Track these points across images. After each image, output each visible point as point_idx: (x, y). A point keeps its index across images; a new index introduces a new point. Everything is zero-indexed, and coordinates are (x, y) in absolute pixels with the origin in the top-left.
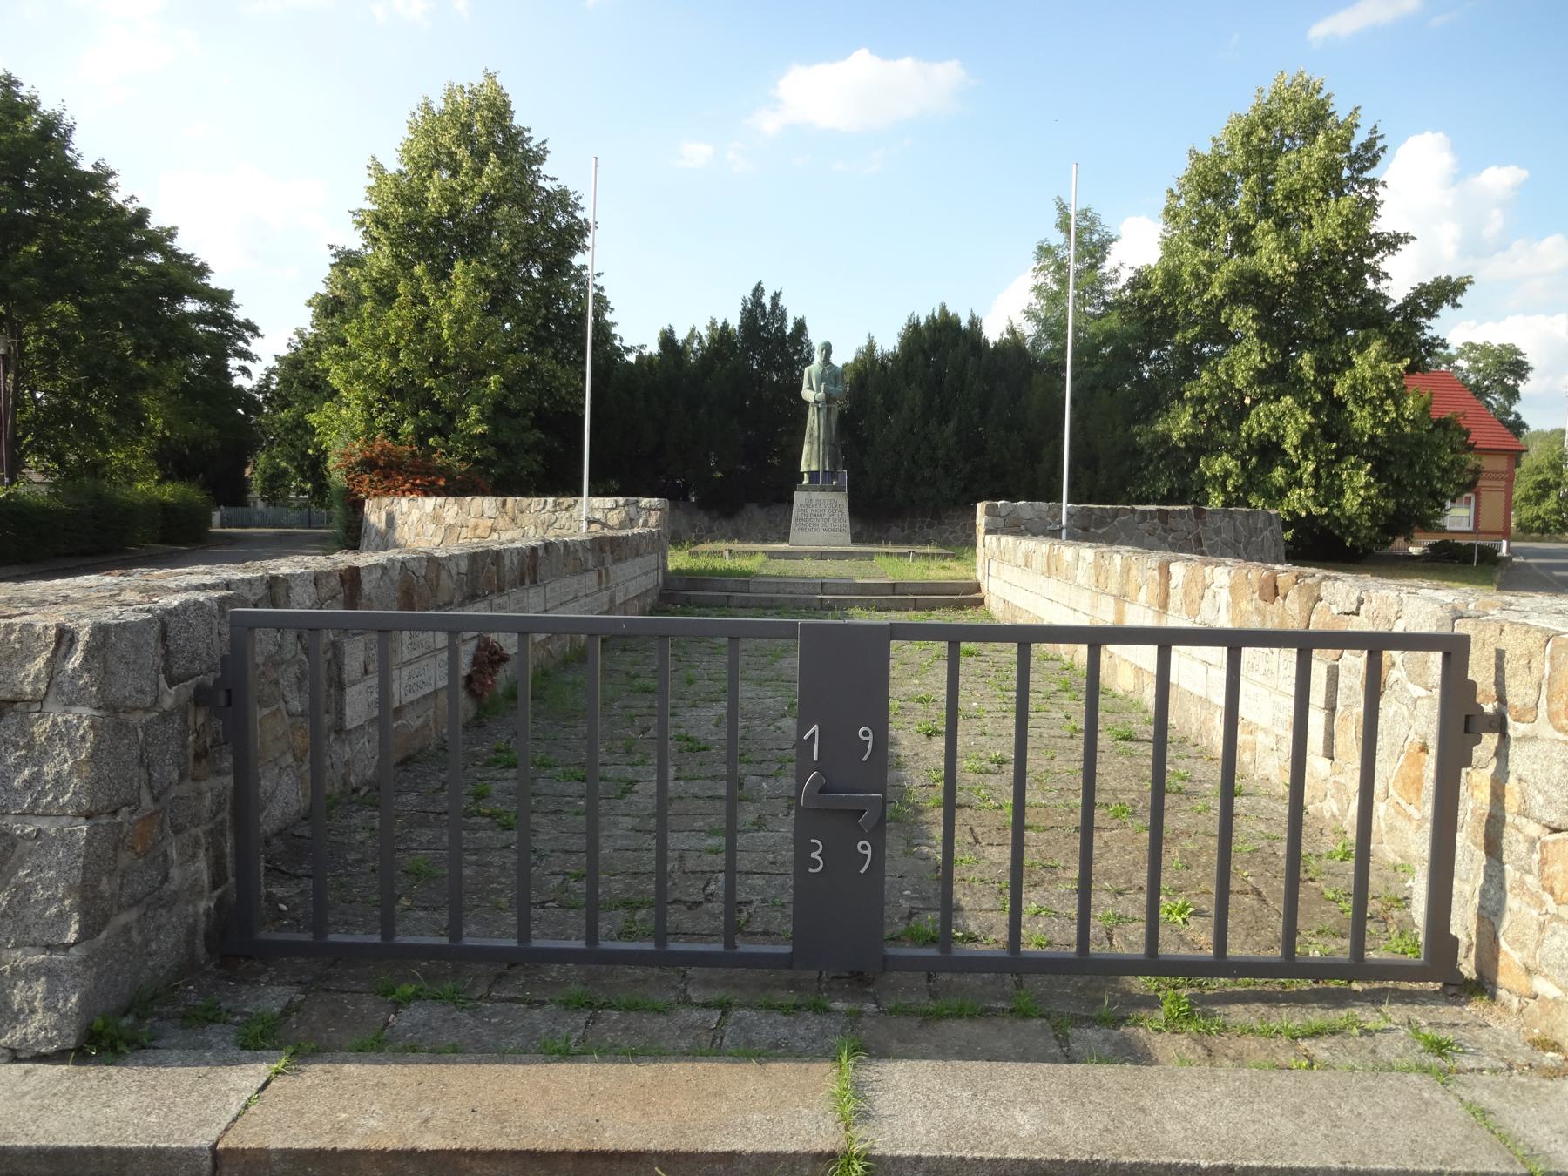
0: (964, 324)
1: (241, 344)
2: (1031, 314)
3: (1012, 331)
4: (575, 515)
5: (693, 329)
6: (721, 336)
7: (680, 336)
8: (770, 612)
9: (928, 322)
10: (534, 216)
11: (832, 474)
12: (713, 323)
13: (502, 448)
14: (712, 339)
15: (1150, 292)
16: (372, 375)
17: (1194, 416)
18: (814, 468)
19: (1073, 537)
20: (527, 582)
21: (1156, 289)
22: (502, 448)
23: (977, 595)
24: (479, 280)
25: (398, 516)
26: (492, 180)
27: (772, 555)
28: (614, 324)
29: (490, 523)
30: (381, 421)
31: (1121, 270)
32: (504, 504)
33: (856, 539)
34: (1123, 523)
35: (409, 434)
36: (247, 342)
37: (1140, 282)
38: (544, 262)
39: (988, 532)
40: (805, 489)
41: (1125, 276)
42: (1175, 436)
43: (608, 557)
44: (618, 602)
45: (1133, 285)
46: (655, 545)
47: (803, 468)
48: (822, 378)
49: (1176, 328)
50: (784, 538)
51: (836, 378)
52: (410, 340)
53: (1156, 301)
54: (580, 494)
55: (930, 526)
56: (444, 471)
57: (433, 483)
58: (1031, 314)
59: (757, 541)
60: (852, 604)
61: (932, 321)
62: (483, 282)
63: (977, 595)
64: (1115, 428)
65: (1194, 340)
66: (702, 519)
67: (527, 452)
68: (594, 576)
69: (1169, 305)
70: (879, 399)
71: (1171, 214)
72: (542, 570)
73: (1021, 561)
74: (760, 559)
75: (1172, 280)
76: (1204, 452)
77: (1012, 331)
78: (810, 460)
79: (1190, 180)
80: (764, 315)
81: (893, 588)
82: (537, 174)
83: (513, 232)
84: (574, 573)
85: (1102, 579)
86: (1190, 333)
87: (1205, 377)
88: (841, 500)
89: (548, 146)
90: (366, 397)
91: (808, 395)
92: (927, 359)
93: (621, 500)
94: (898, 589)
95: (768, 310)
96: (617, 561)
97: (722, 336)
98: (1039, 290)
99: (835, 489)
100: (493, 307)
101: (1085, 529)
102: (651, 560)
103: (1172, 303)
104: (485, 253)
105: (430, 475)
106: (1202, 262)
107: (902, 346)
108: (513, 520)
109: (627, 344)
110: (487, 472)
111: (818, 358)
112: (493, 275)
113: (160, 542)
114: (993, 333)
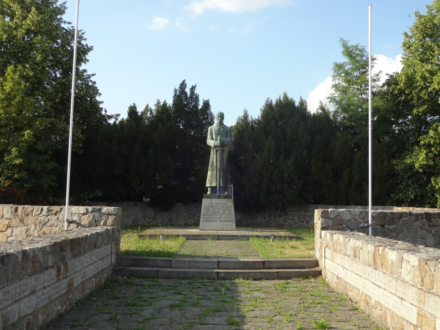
0: (297, 104)
2: (332, 99)
3: (322, 108)
4: (60, 218)
5: (147, 106)
6: (163, 110)
7: (140, 109)
8: (211, 178)
9: (277, 103)
10: (58, 43)
11: (225, 188)
12: (159, 103)
13: (32, 172)
14: (158, 111)
15: (398, 87)
17: (427, 154)
18: (214, 185)
19: (375, 234)
21: (402, 85)
22: (32, 172)
23: (316, 269)
24: (22, 77)
26: (33, 22)
27: (188, 237)
28: (102, 102)
29: (7, 222)
31: (380, 75)
32: (16, 210)
33: (239, 224)
34: (405, 222)
37: (392, 81)
38: (62, 68)
39: (323, 228)
40: (209, 197)
41: (384, 79)
42: (417, 165)
43: (68, 254)
44: (75, 284)
45: (388, 83)
46: (112, 237)
47: (208, 185)
48: (218, 133)
49: (413, 106)
50: (196, 225)
51: (226, 133)
53: (401, 92)
54: (65, 205)
55: (280, 216)
58: (332, 99)
59: (180, 226)
60: (237, 275)
61: (279, 102)
62: (26, 78)
63: (316, 269)
64: (383, 161)
65: (425, 113)
66: (151, 213)
67: (48, 174)
68: (54, 272)
69: (409, 94)
70: (251, 145)
71: (407, 46)
73: (351, 253)
74: (181, 240)
75: (410, 80)
76: (433, 174)
77: (322, 108)
78: (211, 180)
79: (417, 28)
80: (186, 98)
81: (263, 264)
82: (60, 20)
83: (43, 51)
84: (35, 272)
85: (427, 280)
86: (421, 109)
87: (431, 133)
88: (230, 204)
89: (66, 5)
91: (210, 142)
92: (277, 123)
93: (90, 208)
94: (267, 265)
95: (188, 96)
96: (75, 256)
97: (163, 109)
98: (336, 86)
99: (226, 197)
100: (30, 93)
101: (382, 226)
102: (106, 249)
103: (410, 93)
104: (27, 62)
106: (427, 70)
107: (263, 116)
108: (22, 220)
109: (109, 113)
111: (216, 121)
112: (31, 74)
114: (313, 108)
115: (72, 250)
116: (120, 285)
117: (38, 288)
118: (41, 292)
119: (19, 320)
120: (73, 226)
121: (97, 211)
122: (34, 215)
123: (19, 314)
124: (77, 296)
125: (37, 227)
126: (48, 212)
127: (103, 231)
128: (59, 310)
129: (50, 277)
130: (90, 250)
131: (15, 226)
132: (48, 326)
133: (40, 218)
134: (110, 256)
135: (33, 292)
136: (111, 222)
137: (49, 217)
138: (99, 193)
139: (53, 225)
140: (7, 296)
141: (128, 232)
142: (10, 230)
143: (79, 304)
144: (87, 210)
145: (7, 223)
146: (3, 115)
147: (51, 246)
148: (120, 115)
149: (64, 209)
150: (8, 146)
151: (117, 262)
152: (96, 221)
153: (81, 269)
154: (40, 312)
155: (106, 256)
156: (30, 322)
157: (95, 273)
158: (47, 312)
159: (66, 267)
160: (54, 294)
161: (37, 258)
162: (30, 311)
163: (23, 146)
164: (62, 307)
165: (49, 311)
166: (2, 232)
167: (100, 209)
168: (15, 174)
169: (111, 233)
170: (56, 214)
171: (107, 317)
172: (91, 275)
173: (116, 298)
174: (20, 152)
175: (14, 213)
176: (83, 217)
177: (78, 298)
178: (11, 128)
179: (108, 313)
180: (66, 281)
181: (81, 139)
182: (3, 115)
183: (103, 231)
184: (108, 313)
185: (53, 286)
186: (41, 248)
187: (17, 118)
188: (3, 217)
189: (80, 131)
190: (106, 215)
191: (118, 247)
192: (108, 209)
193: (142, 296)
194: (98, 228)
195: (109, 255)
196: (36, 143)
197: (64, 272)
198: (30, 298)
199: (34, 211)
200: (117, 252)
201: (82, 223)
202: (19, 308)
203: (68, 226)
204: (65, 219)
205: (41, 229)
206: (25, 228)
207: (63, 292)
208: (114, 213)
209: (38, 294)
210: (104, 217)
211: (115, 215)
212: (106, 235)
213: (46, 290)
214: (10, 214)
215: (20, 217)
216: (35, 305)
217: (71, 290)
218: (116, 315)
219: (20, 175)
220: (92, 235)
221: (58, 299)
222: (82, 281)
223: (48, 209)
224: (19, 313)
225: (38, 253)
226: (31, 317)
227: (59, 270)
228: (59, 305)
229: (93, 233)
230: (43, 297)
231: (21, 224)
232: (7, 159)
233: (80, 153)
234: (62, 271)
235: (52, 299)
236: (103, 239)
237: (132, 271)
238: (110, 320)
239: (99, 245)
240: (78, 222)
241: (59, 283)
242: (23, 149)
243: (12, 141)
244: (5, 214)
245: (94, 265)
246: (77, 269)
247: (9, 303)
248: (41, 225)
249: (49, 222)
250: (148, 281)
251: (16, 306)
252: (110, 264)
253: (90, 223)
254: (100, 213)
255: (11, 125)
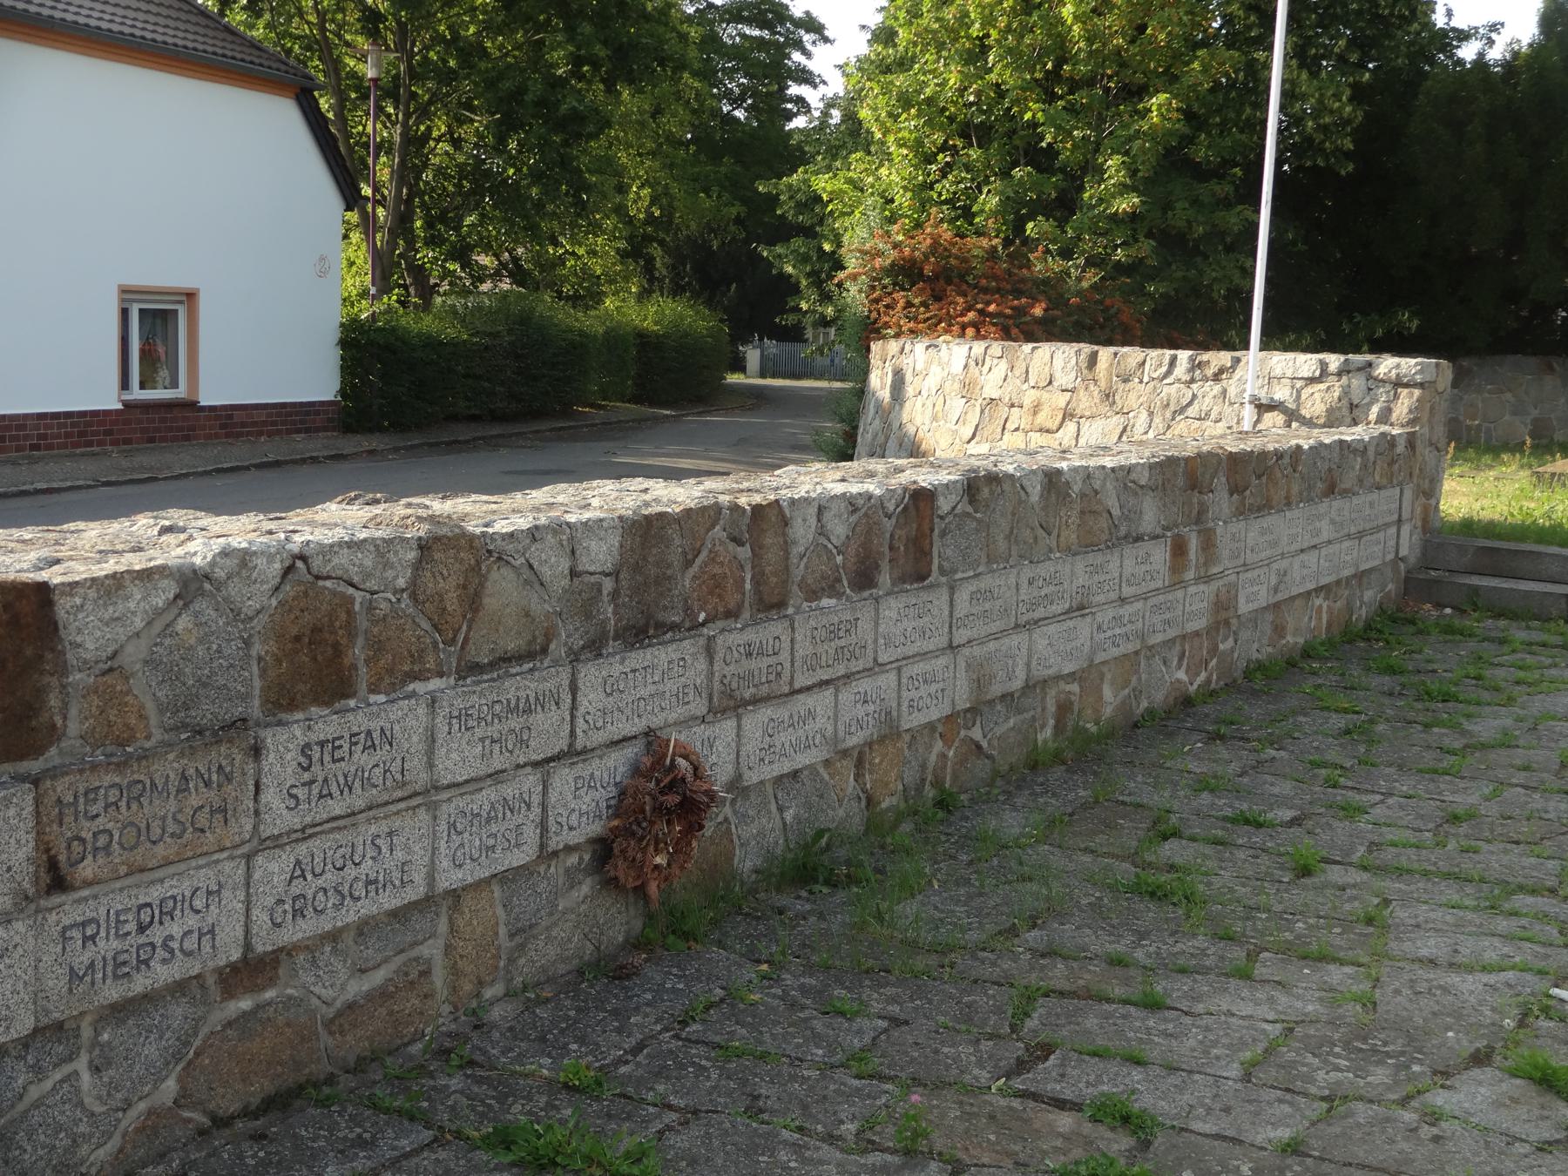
1: (797, 56)
4: (1232, 392)
16: (930, 101)
20: (885, 578)
25: (909, 377)
29: (1062, 400)
30: (946, 187)
32: (1093, 360)
35: (994, 214)
36: (808, 54)
46: (1404, 465)
52: (1008, 29)
54: (1247, 347)
56: (1050, 288)
57: (1020, 312)
68: (1160, 555)
72: (942, 550)
84: (1088, 545)
90: (919, 143)
93: (1334, 361)
96: (1241, 512)
102: (1383, 503)
105: (1018, 293)
108: (1108, 396)
109: (1459, 22)
110: (1141, 291)
113: (636, 399)
115: (1234, 489)
116: (1420, 632)
117: (1100, 598)
118: (1111, 613)
119: (1028, 687)
120: (1273, 419)
121: (1359, 369)
122: (1146, 379)
123: (1029, 670)
124: (1253, 646)
125: (1157, 420)
126: (1192, 370)
127: (1367, 438)
128: (1178, 681)
129: (1144, 568)
130: (1310, 500)
131: (1087, 413)
132: (1136, 726)
133: (1166, 390)
134: (1393, 530)
135: (1081, 607)
136: (1405, 411)
137: (1194, 386)
138: (1409, 321)
139: (1208, 414)
140: (987, 606)
141: (1503, 463)
142: (1071, 427)
143: (1258, 675)
144: (1323, 365)
145: (1063, 405)
146: (1082, 44)
147: (1151, 467)
148: (1502, 25)
149: (1244, 360)
150: (1097, 150)
151: (1424, 554)
152: (1352, 407)
153: (1270, 562)
154: (1108, 676)
155: (1378, 529)
156: (1072, 703)
157: (1324, 581)
158: (1134, 680)
159: (1208, 544)
160: (1159, 627)
161: (1099, 502)
162: (1068, 668)
163: (1142, 149)
164: (1193, 672)
165: (1140, 679)
166: (1048, 431)
167: (1370, 365)
168: (1116, 247)
169: (1400, 449)
170: (1217, 377)
171: (1338, 722)
172: (1311, 586)
173: (1391, 670)
174: (1133, 173)
175: (1085, 372)
176: (1309, 390)
177: (1255, 656)
178: (1107, 90)
179: (1345, 711)
180: (1208, 590)
181: (1349, 122)
182: (1082, 44)
183: (1367, 438)
184: (1345, 711)
185: (1151, 602)
186: (1113, 469)
187: (1127, 50)
188: (1050, 383)
189: (1348, 92)
190: (1388, 387)
191: (1433, 502)
192: (1398, 366)
193: (1487, 673)
194: (1359, 429)
195: (1387, 525)
196: (1189, 140)
197: (1202, 561)
198: (1071, 624)
199: (1147, 366)
200: (1425, 521)
201: (1303, 412)
202: (1030, 649)
203: (1258, 421)
204: (1247, 395)
205: (1169, 427)
206: (1116, 423)
207: (1199, 624)
208: (1418, 378)
209: (1099, 619)
210: (1383, 394)
211: (1421, 385)
212: (1378, 454)
213: (1127, 610)
214: (1073, 374)
215: (1103, 384)
216: (1086, 649)
217: (1227, 623)
218: (1372, 721)
219: (1133, 252)
220: (1318, 448)
221: (1178, 647)
222: (1272, 600)
223: (1192, 359)
224: (1028, 665)
225: (1104, 485)
226: (1075, 688)
227: (1179, 549)
228: (1179, 667)
229: (1327, 441)
230: (1117, 631)
231: (1105, 409)
232: (1091, 198)
233: (1343, 173)
234: (1192, 555)
235: (1151, 642)
236: (1364, 467)
237: (1476, 590)
238: (1348, 732)
239: (1346, 485)
240: (1292, 406)
241: (1180, 594)
242: (1143, 163)
243: (1111, 133)
244: (1058, 374)
245: (1324, 552)
246: (1250, 558)
247: (994, 627)
248: (1168, 415)
249: (1196, 405)
250: (1528, 628)
251: (1015, 640)
252: (1390, 556)
253: (1330, 411)
254: (1369, 377)
255: (1110, 78)
